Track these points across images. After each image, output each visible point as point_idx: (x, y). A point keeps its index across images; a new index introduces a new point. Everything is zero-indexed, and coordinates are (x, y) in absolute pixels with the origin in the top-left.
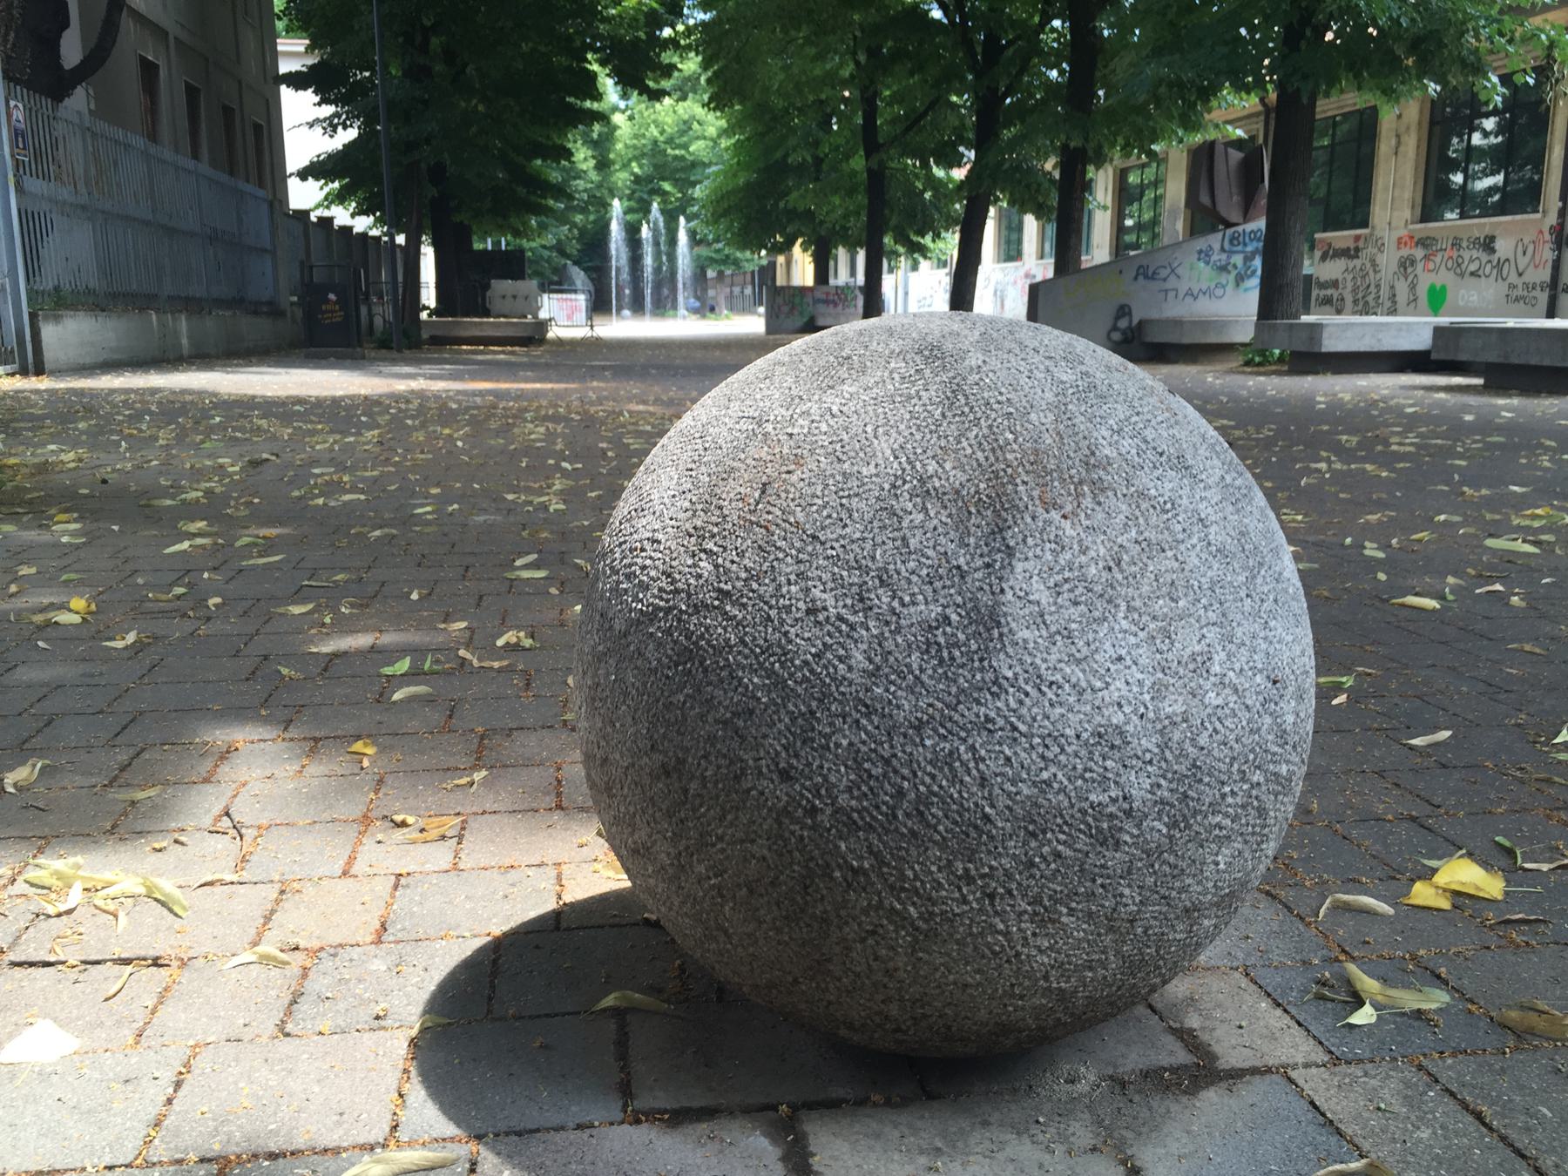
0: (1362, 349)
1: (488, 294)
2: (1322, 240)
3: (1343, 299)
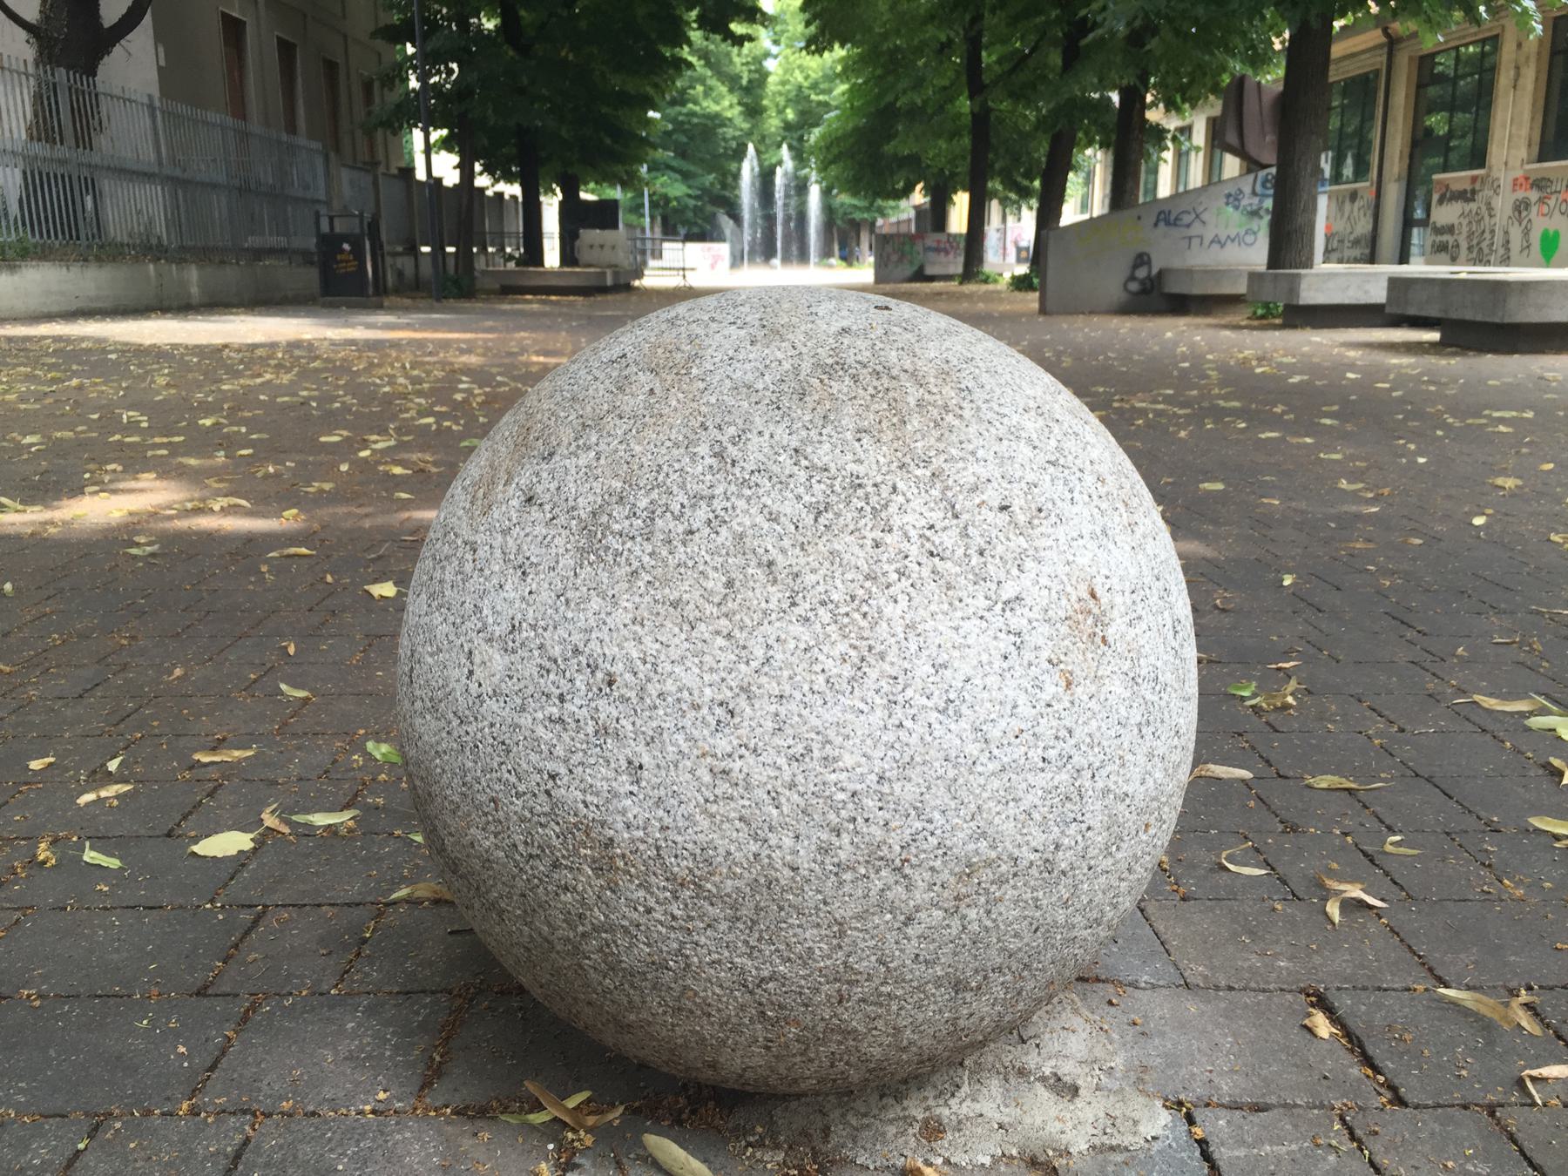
0: (1347, 301)
1: (577, 243)
2: (1439, 182)
3: (1458, 246)
